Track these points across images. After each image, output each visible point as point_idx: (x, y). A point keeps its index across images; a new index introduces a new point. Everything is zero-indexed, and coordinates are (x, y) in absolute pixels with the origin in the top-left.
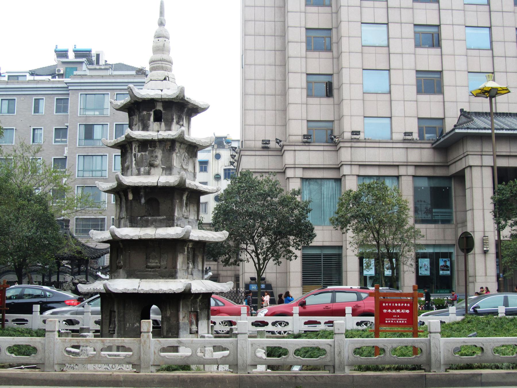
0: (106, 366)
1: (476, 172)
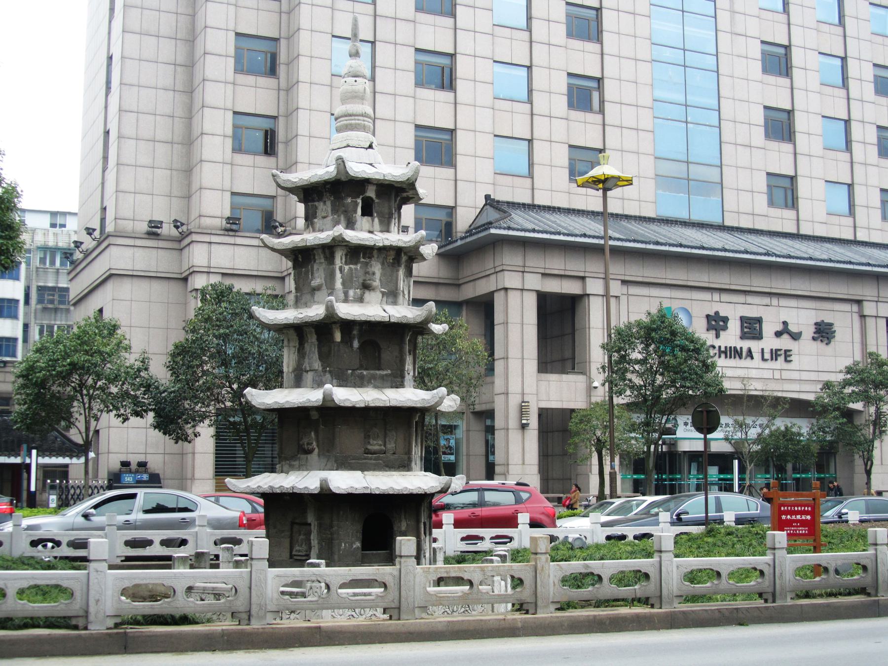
0: (350, 612)
1: (514, 297)
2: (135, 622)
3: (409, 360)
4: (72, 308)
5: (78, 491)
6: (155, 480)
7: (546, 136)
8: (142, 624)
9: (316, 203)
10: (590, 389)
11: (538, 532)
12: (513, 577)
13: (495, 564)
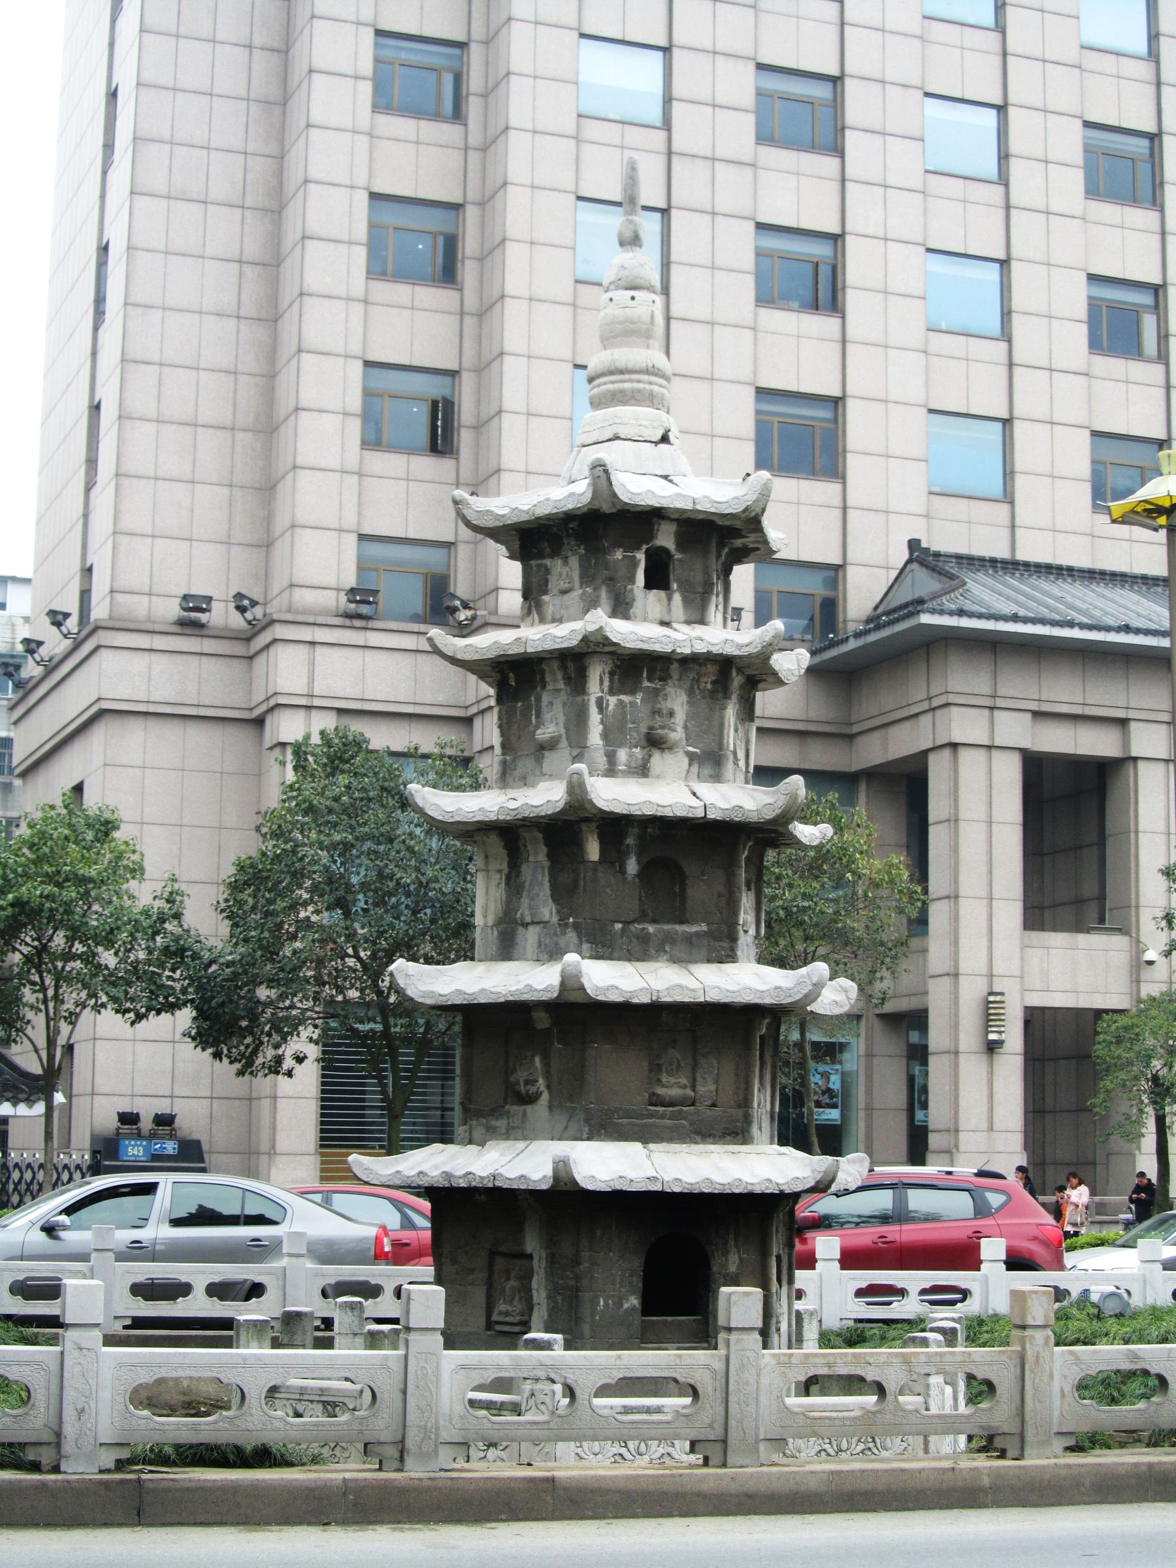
0: (617, 1449)
2: (160, 1458)
3: (747, 901)
4: (18, 782)
5: (28, 1176)
6: (191, 1155)
7: (1041, 412)
8: (174, 1464)
9: (548, 562)
10: (1139, 965)
11: (1024, 1280)
12: (970, 1377)
13: (933, 1349)
